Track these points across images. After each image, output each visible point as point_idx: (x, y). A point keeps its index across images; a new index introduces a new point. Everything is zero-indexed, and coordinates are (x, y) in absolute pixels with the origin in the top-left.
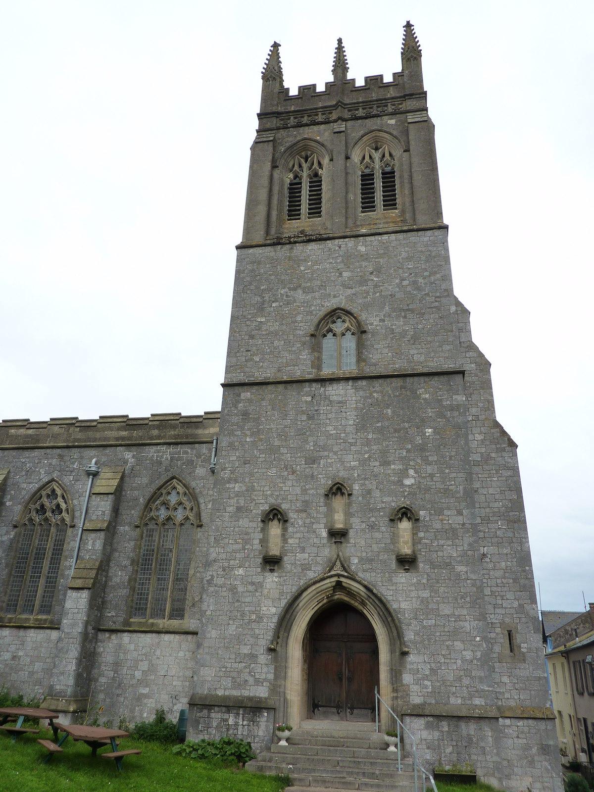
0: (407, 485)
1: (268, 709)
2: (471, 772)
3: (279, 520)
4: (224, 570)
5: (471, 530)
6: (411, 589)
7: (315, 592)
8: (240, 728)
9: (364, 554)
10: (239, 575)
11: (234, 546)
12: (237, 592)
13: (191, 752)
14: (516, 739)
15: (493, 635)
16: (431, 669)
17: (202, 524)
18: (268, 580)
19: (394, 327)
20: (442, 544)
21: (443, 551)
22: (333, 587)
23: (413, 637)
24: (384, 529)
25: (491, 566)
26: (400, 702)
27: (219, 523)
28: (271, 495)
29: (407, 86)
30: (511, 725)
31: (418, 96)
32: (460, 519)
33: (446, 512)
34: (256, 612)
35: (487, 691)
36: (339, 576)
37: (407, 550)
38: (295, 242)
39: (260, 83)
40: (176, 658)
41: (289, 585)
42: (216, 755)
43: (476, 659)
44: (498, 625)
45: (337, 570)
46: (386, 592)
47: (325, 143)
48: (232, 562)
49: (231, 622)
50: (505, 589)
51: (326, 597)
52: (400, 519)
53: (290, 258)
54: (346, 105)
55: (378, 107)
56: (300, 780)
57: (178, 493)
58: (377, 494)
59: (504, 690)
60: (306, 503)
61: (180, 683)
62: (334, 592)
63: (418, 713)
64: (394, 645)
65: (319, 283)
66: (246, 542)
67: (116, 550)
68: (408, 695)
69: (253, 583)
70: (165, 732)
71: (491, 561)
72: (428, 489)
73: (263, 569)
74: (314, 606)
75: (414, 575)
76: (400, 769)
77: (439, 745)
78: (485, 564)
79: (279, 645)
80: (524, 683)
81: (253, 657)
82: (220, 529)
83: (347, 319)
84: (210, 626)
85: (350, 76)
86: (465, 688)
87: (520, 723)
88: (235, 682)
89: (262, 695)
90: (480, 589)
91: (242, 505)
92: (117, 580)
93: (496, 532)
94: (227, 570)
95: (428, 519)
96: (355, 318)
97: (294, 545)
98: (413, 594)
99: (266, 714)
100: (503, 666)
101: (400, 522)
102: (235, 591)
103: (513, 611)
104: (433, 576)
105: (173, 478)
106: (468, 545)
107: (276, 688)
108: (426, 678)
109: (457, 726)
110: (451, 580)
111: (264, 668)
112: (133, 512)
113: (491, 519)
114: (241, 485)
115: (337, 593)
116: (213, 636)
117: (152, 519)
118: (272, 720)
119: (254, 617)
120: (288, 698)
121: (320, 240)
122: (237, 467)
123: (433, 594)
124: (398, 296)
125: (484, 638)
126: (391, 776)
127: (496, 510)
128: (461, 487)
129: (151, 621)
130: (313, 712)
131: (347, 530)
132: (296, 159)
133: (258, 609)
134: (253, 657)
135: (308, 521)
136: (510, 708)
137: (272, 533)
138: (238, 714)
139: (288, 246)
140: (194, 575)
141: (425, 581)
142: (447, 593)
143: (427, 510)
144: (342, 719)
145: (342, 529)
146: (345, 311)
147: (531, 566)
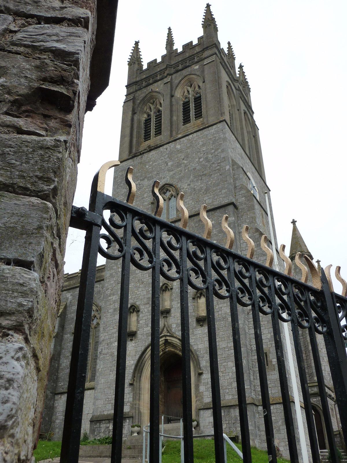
11: (113, 330)
19: (195, 187)
20: (221, 307)
23: (205, 364)
29: (205, 43)
31: (211, 47)
36: (165, 336)
38: (143, 153)
39: (127, 67)
47: (161, 91)
49: (111, 373)
53: (141, 163)
54: (171, 65)
55: (190, 61)
65: (156, 173)
67: (63, 349)
68: (202, 398)
79: (135, 381)
83: (171, 189)
85: (175, 48)
86: (234, 389)
92: (64, 365)
96: (174, 187)
99: (128, 421)
101: (200, 299)
109: (229, 412)
110: (226, 326)
112: (71, 326)
120: (142, 411)
121: (156, 148)
122: (114, 287)
124: (198, 168)
132: (148, 106)
139: (140, 156)
146: (169, 185)
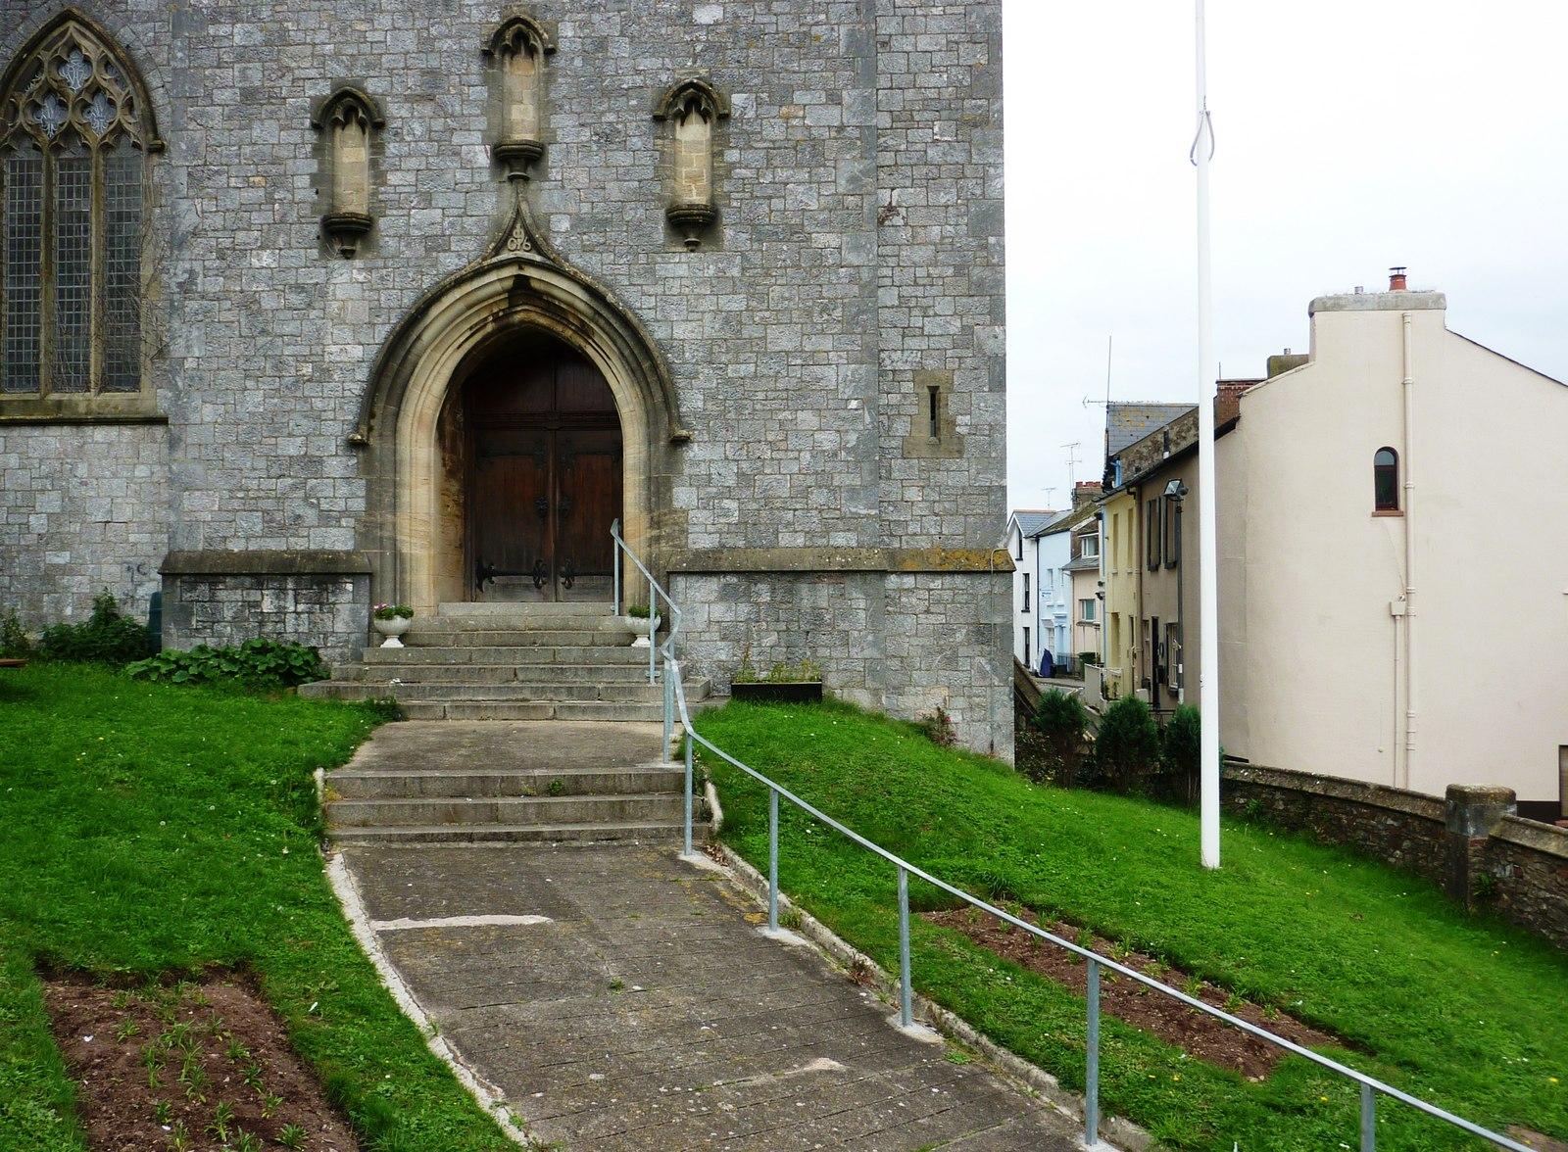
0: (701, 25)
1: (354, 576)
2: (811, 679)
3: (362, 124)
4: (222, 257)
5: (859, 143)
6: (703, 291)
7: (460, 306)
8: (290, 619)
9: (586, 208)
10: (263, 268)
12: (260, 311)
13: (171, 673)
14: (924, 616)
15: (894, 399)
16: (740, 475)
17: (163, 145)
18: (339, 280)
21: (784, 197)
22: (508, 291)
23: (700, 404)
24: (636, 142)
25: (904, 235)
26: (664, 547)
27: (198, 135)
28: (336, 56)
30: (916, 588)
32: (833, 115)
33: (799, 97)
34: (313, 358)
35: (865, 516)
36: (521, 262)
37: (695, 196)
40: (130, 480)
41: (394, 288)
42: (232, 674)
43: (845, 448)
44: (909, 375)
45: (518, 248)
46: (640, 301)
48: (241, 236)
49: (250, 384)
50: (934, 291)
51: (491, 318)
52: (683, 117)
56: (421, 708)
57: (87, 61)
58: (622, 49)
59: (909, 518)
60: (432, 75)
61: (146, 538)
62: (511, 306)
63: (704, 568)
64: (656, 423)
66: (275, 183)
68: (685, 532)
69: (300, 288)
70: (116, 642)
71: (906, 225)
72: (755, 37)
73: (325, 251)
74: (462, 339)
75: (711, 256)
76: (652, 680)
77: (749, 630)
78: (892, 230)
79: (375, 433)
80: (955, 501)
81: (312, 463)
82: (202, 149)
84: (197, 395)
87: (937, 583)
88: (271, 521)
89: (339, 547)
90: (872, 288)
91: (258, 84)
93: (926, 152)
94: (230, 256)
95: (751, 114)
97: (402, 189)
98: (707, 304)
99: (349, 587)
100: (911, 467)
101: (682, 125)
102: (255, 307)
103: (947, 343)
104: (757, 259)
105: (66, 17)
106: (848, 181)
107: (375, 527)
108: (727, 493)
109: (790, 592)
110: (799, 267)
111: (340, 485)
113: (917, 118)
114: (249, 27)
115: (519, 309)
116: (207, 419)
117: (21, 134)
118: (365, 599)
119: (307, 369)
120: (405, 550)
123: (754, 304)
125: (868, 403)
126: (631, 691)
127: (932, 94)
128: (843, 30)
129: (54, 396)
130: (479, 586)
131: (543, 147)
133: (318, 349)
134: (312, 463)
135: (438, 124)
136: (918, 554)
137: (345, 160)
138: (283, 590)
140: (154, 278)
141: (735, 272)
142: (789, 299)
143: (750, 91)
144: (546, 599)
145: (527, 143)
147: (1001, 234)
